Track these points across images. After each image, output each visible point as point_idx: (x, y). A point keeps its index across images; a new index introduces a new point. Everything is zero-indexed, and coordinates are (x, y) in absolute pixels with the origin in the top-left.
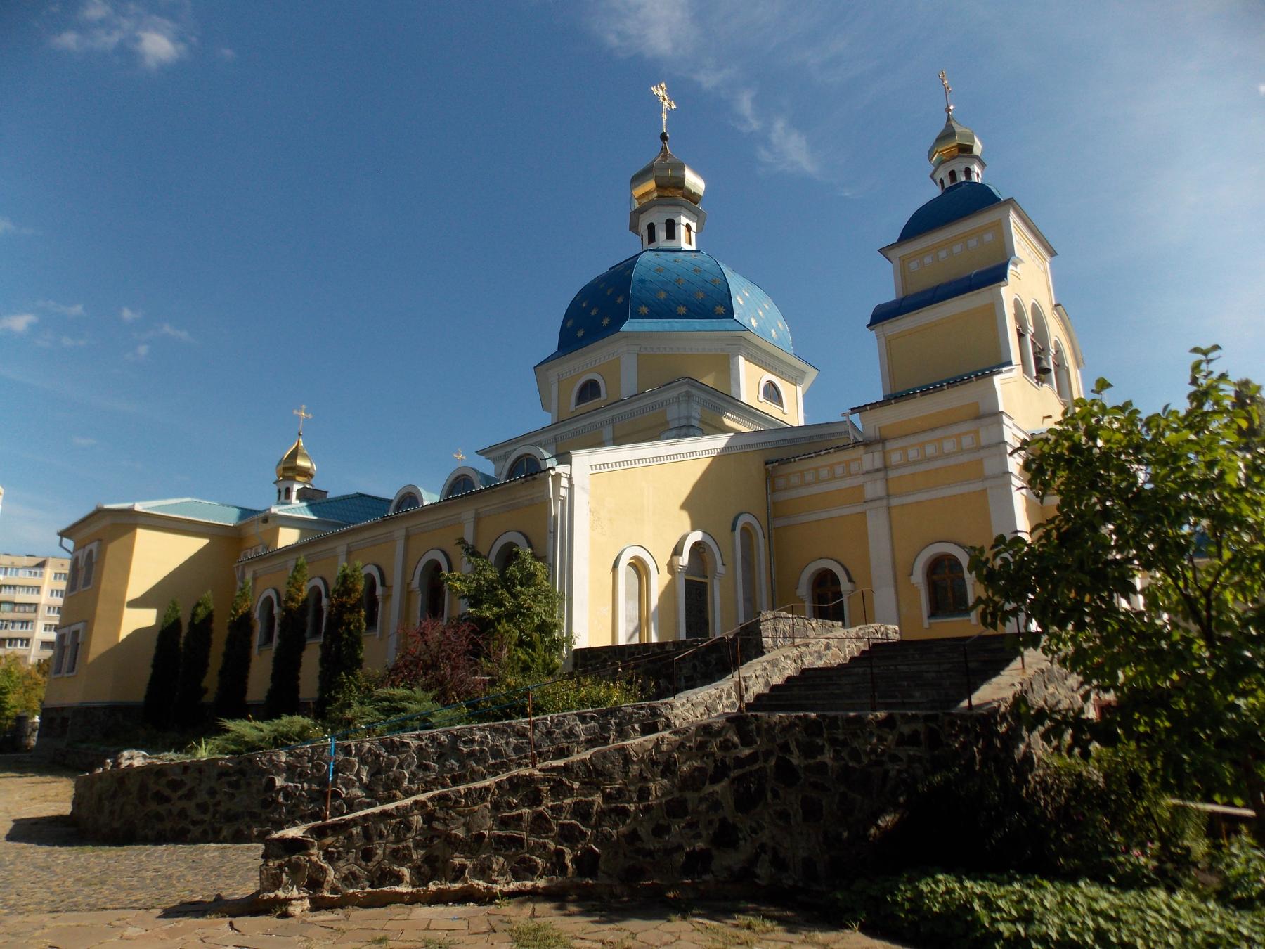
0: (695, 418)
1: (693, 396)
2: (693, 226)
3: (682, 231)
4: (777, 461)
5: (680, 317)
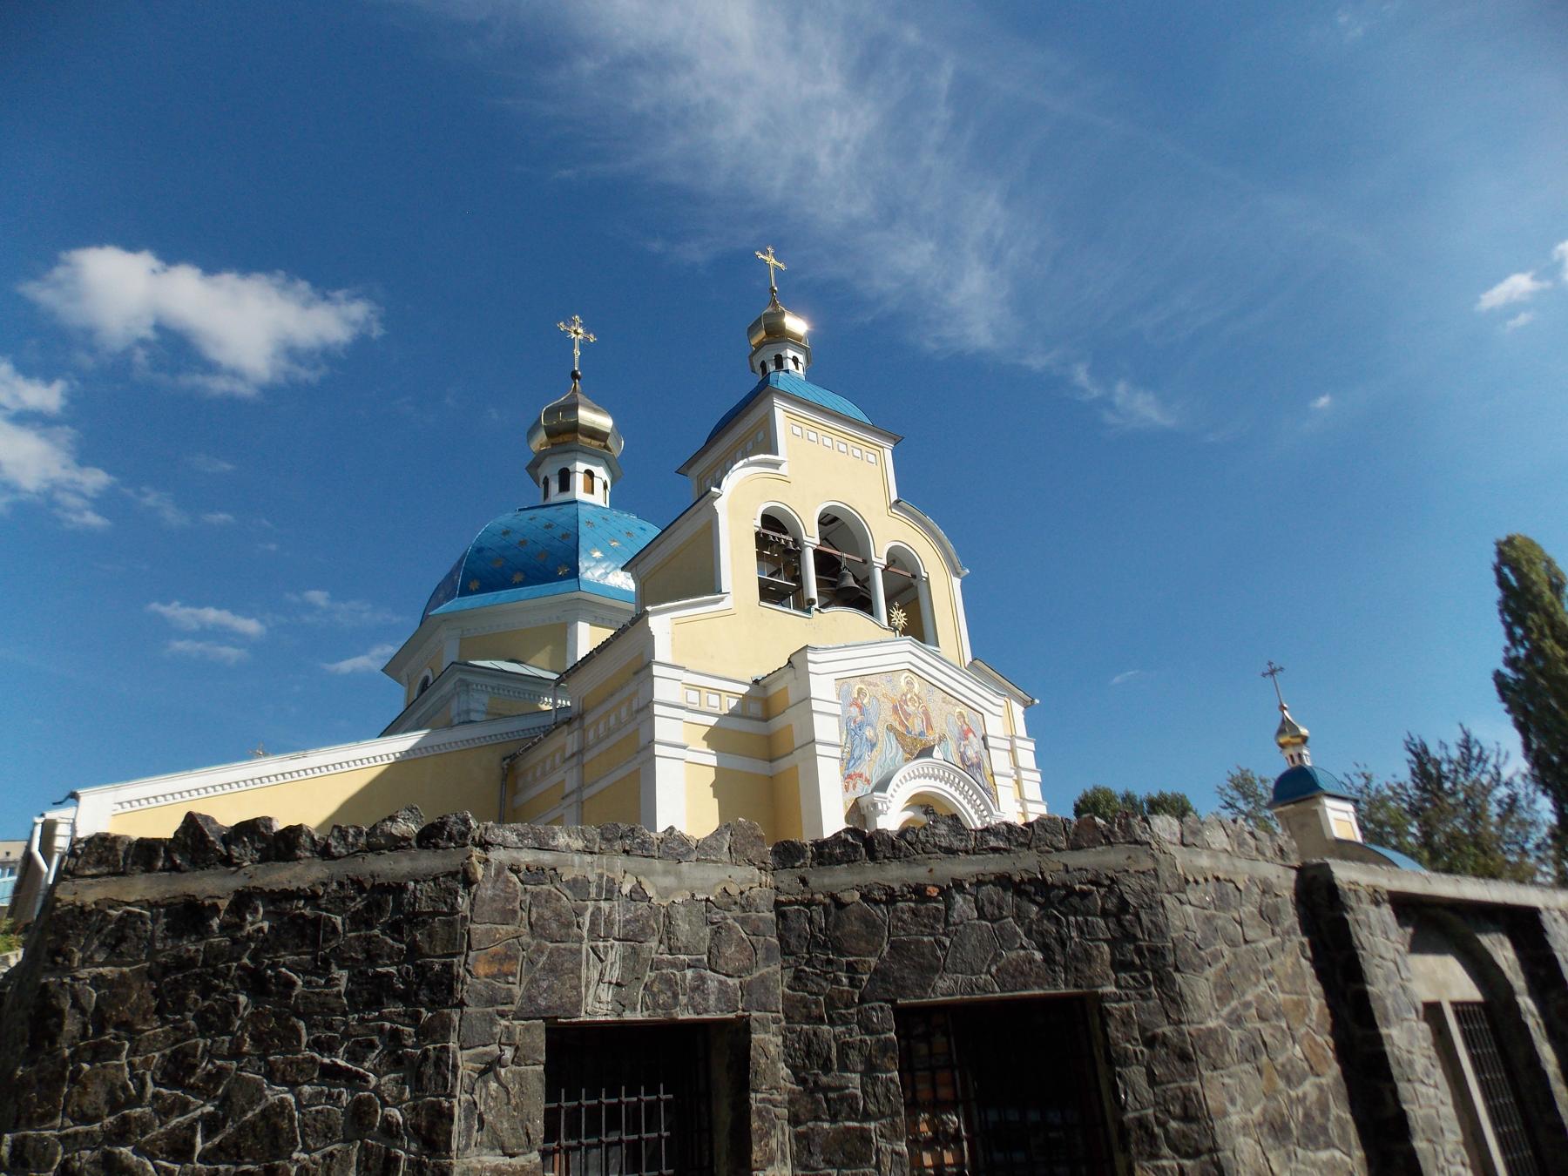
0: (477, 711)
2: (801, 358)
3: (579, 481)
5: (516, 585)
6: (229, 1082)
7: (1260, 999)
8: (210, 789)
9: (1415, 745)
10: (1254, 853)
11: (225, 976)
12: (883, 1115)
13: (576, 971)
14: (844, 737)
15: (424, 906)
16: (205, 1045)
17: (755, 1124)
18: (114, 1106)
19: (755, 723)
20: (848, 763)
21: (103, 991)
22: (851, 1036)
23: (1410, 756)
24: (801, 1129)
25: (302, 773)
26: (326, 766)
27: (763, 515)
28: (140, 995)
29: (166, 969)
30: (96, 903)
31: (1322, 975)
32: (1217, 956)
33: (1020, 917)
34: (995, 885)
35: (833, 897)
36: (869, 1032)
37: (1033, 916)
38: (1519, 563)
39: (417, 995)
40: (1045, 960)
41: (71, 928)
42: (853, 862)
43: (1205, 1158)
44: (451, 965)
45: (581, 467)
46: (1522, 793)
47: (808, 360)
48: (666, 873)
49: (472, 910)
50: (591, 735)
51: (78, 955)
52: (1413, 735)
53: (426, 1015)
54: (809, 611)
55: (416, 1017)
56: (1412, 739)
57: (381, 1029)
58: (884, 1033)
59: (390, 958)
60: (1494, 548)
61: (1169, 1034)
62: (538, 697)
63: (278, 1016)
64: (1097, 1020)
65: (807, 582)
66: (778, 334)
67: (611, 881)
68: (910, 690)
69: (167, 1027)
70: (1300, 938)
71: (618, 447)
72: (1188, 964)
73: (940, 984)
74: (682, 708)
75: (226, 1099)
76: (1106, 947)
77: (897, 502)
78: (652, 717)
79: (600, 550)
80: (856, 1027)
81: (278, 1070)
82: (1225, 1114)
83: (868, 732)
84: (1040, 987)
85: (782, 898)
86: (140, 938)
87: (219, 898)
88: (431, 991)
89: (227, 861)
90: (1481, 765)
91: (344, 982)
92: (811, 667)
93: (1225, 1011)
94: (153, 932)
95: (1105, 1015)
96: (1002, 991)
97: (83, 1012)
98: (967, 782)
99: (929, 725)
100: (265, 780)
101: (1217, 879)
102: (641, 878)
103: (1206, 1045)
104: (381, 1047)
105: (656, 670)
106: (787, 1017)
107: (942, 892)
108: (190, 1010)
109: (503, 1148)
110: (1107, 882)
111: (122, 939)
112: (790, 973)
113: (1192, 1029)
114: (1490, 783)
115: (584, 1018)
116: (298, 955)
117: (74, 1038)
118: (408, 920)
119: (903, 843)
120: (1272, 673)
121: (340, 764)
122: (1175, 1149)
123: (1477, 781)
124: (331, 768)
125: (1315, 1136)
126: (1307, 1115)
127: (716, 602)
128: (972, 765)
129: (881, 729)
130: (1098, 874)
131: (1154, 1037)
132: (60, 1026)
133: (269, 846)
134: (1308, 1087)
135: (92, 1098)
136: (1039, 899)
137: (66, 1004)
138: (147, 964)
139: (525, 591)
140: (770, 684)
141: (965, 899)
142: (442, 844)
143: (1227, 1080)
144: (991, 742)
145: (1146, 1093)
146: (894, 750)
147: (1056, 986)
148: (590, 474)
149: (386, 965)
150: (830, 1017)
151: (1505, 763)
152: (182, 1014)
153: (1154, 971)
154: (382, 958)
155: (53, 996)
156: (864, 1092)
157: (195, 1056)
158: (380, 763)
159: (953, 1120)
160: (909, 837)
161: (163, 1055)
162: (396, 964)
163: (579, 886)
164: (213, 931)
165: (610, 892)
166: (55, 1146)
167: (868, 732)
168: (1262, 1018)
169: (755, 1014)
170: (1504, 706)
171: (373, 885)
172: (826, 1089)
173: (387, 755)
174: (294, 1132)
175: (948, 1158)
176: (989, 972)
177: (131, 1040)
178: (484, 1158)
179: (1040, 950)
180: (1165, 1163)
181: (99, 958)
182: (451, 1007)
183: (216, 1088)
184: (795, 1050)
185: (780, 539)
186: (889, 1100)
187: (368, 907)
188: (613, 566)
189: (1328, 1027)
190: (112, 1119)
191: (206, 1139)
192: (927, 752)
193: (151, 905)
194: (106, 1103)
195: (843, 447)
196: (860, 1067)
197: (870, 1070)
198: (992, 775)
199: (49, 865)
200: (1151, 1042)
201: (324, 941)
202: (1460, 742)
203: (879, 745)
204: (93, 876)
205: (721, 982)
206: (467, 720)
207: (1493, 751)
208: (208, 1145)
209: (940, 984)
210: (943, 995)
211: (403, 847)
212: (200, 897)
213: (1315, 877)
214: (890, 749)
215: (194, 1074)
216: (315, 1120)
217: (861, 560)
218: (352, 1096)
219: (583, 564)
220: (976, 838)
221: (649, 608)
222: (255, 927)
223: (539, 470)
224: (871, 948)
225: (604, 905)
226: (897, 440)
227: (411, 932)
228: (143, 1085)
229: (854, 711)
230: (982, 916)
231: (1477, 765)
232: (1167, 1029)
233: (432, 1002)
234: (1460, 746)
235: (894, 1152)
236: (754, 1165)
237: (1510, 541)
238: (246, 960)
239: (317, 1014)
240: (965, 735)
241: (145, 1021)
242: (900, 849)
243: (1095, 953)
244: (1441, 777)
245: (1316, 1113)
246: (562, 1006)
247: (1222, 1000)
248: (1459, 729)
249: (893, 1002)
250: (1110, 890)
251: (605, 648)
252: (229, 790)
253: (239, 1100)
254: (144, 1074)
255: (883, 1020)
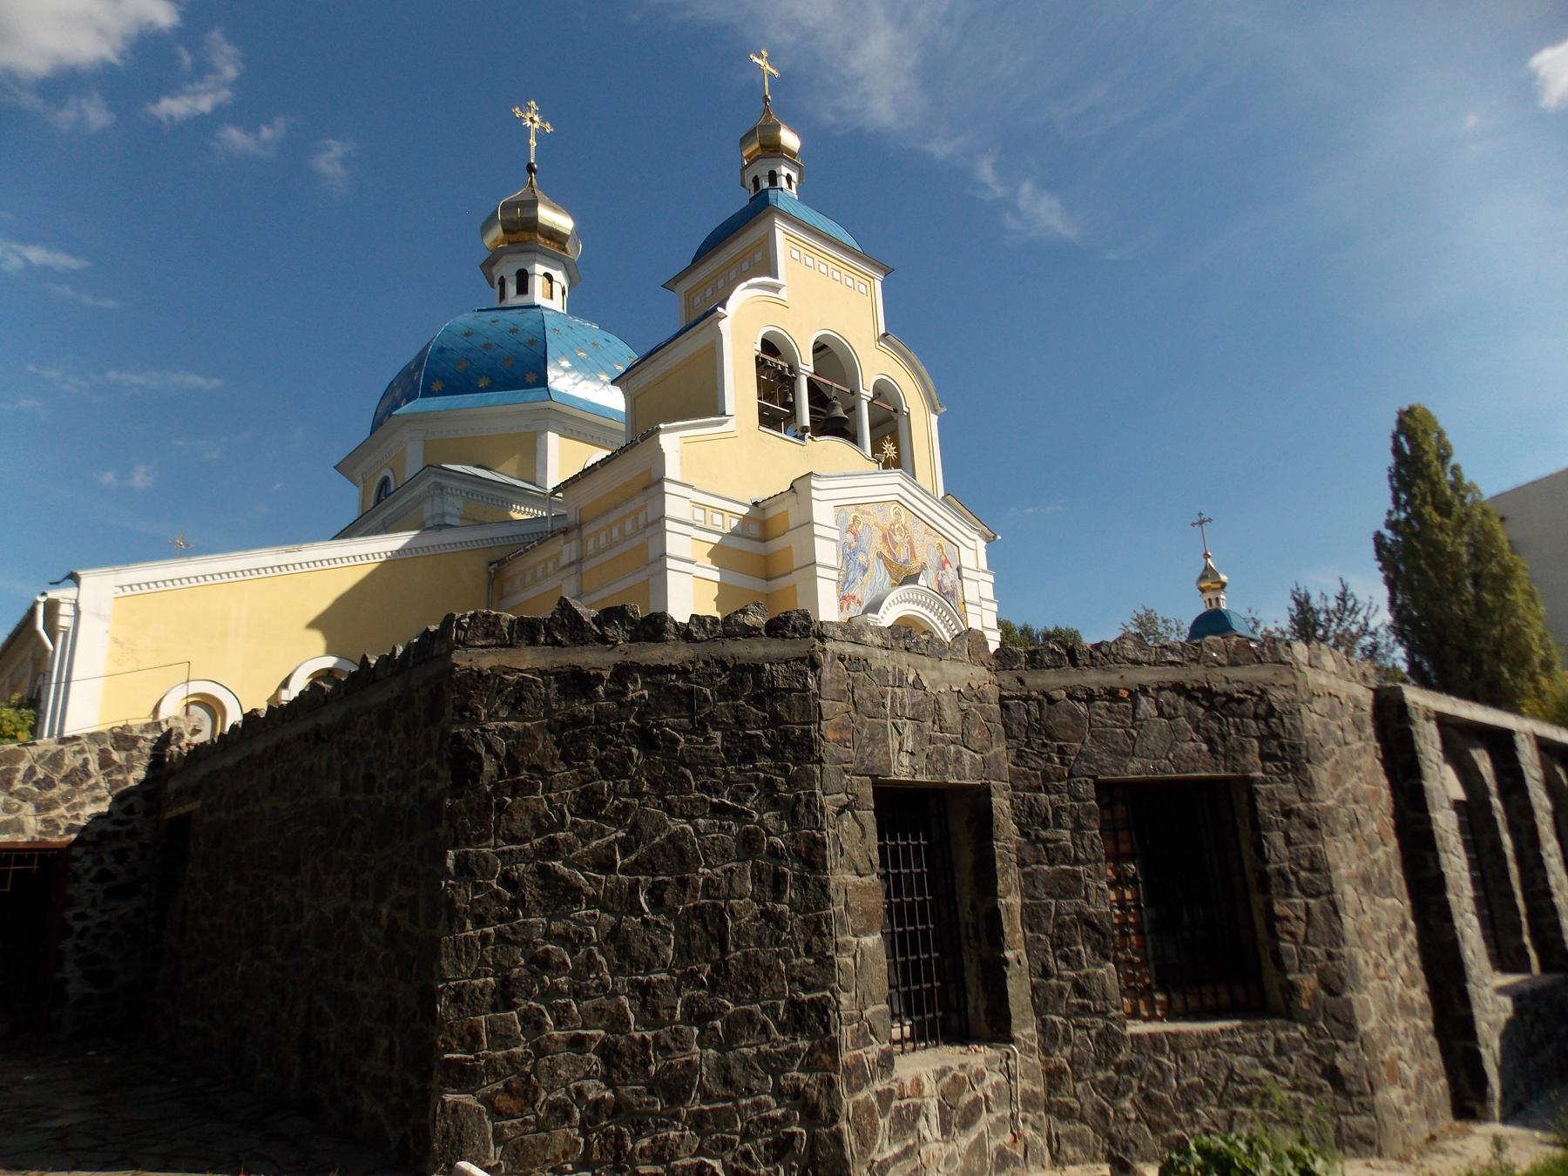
0: (452, 515)
1: (447, 487)
2: (794, 177)
3: (538, 284)
4: (498, 562)
5: (482, 390)
6: (636, 815)
7: (1355, 787)
8: (209, 578)
9: (1300, 595)
10: (1349, 676)
11: (617, 733)
12: (1089, 861)
13: (885, 740)
14: (840, 561)
15: (781, 683)
16: (609, 785)
17: (999, 864)
18: (541, 831)
19: (754, 543)
20: (843, 585)
21: (510, 741)
22: (1063, 802)
23: (1292, 604)
24: (1027, 869)
25: (297, 566)
26: (321, 561)
27: (763, 340)
28: (545, 744)
29: (564, 726)
30: (490, 669)
31: (1389, 773)
32: (1332, 752)
33: (1190, 717)
34: (1170, 690)
35: (1045, 694)
36: (1077, 799)
37: (1200, 717)
38: (1416, 433)
39: (782, 753)
40: (1209, 751)
41: (472, 688)
42: (1059, 667)
43: (1324, 898)
44: (810, 730)
45: (540, 269)
46: (1383, 642)
47: (800, 178)
48: (933, 668)
49: (819, 689)
50: (590, 545)
51: (484, 711)
52: (1300, 586)
53: (793, 768)
54: (802, 438)
55: (785, 770)
56: (1298, 589)
57: (757, 779)
58: (1088, 800)
59: (755, 723)
60: (1396, 417)
61: (1302, 808)
62: (507, 505)
63: (668, 766)
64: (1245, 797)
65: (801, 412)
66: (774, 149)
67: (901, 672)
68: (898, 521)
69: (574, 771)
70: (1374, 744)
71: (575, 251)
72: (1316, 757)
73: (1131, 765)
74: (691, 525)
75: (635, 827)
76: (1256, 743)
77: (885, 335)
78: (663, 531)
79: (567, 359)
80: (1067, 796)
81: (676, 806)
82: (1337, 867)
83: (861, 558)
84: (1206, 770)
85: (1005, 693)
86: (536, 699)
87: (601, 669)
88: (795, 750)
89: (603, 639)
90: (1353, 616)
91: (719, 740)
92: (814, 493)
93: (1336, 794)
94: (547, 695)
95: (1252, 794)
96: (1178, 772)
97: (497, 756)
98: (945, 608)
99: (913, 555)
100: (262, 571)
101: (1330, 694)
102: (919, 671)
103: (1327, 818)
104: (758, 792)
105: (668, 487)
106: (1013, 786)
107: (1132, 694)
108: (591, 758)
109: (857, 870)
110: (1258, 692)
111: (521, 699)
112: (1013, 753)
113: (1318, 805)
114: (1357, 634)
115: (894, 778)
116: (677, 718)
117: (492, 777)
118: (766, 694)
119: (1099, 654)
120: (1201, 523)
121: (334, 559)
122: (1303, 892)
123: (1347, 630)
124: (325, 563)
125: (1384, 889)
126: (1381, 874)
127: (720, 423)
128: (948, 593)
129: (872, 556)
130: (1252, 685)
131: (1291, 810)
132: (481, 767)
133: (637, 630)
134: (1380, 854)
135: (519, 824)
136: (1204, 703)
137: (482, 750)
138: (546, 721)
139: (494, 397)
140: (768, 507)
141: (1148, 701)
142: (789, 634)
143: (1339, 845)
144: (965, 573)
145: (1284, 851)
146: (883, 576)
147: (1218, 770)
148: (549, 277)
149: (754, 729)
150: (1046, 787)
151: (1373, 615)
152: (584, 761)
153: (1292, 761)
154: (749, 723)
155: (467, 743)
156: (1074, 843)
157: (603, 794)
158: (372, 561)
159: (1132, 868)
160: (1103, 649)
161: (574, 792)
162: (762, 728)
163: (881, 673)
164: (600, 696)
165: (901, 680)
166: (495, 860)
167: (861, 558)
168: (1356, 801)
169: (993, 782)
170: (1379, 564)
171: (735, 665)
172: (1045, 841)
173: (379, 554)
174: (697, 852)
175: (1128, 895)
176: (1167, 758)
177: (543, 780)
178: (846, 876)
179: (1205, 743)
180: (1296, 901)
181: (503, 714)
182: (812, 763)
183: (626, 818)
184: (1020, 811)
185: (777, 364)
186: (1094, 850)
187: (732, 682)
188: (581, 376)
189: (1391, 811)
190: (540, 840)
191: (624, 856)
192: (912, 579)
193: (542, 673)
194: (532, 828)
195: (836, 275)
196: (1070, 825)
197: (1078, 828)
198: (964, 603)
199: (53, 642)
200: (1288, 813)
201: (699, 707)
202: (1338, 595)
203: (870, 570)
204: (483, 647)
205: (972, 757)
206: (441, 523)
207: (1365, 604)
208: (626, 861)
209: (1131, 765)
210: (1133, 774)
211: (754, 636)
212: (586, 668)
213: (1387, 697)
214: (879, 576)
215: (604, 807)
216: (713, 844)
217: (848, 391)
218: (741, 828)
219: (552, 373)
220: (1156, 653)
221: (662, 426)
222: (637, 694)
223: (494, 270)
224: (1076, 736)
225: (898, 690)
226: (887, 271)
227: (771, 703)
228: (563, 816)
229: (850, 537)
230: (1161, 714)
231: (1349, 616)
232: (1301, 806)
233: (797, 758)
234: (1338, 598)
235: (1098, 888)
236: (999, 894)
237: (1410, 412)
238: (632, 721)
239: (700, 764)
240: (943, 564)
241: (554, 765)
242: (1096, 659)
243: (1248, 746)
244: (1316, 624)
245: (1385, 871)
246: (881, 767)
247: (1335, 786)
248: (1339, 584)
249: (1094, 777)
250: (1261, 698)
251: (609, 462)
252: (227, 580)
253: (647, 829)
254: (562, 806)
255: (1086, 792)
